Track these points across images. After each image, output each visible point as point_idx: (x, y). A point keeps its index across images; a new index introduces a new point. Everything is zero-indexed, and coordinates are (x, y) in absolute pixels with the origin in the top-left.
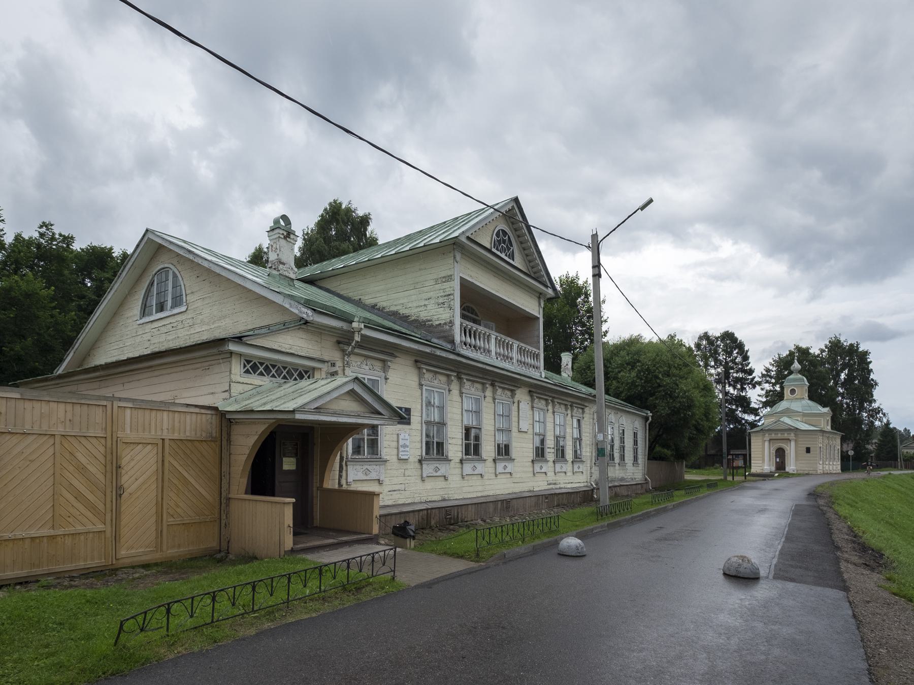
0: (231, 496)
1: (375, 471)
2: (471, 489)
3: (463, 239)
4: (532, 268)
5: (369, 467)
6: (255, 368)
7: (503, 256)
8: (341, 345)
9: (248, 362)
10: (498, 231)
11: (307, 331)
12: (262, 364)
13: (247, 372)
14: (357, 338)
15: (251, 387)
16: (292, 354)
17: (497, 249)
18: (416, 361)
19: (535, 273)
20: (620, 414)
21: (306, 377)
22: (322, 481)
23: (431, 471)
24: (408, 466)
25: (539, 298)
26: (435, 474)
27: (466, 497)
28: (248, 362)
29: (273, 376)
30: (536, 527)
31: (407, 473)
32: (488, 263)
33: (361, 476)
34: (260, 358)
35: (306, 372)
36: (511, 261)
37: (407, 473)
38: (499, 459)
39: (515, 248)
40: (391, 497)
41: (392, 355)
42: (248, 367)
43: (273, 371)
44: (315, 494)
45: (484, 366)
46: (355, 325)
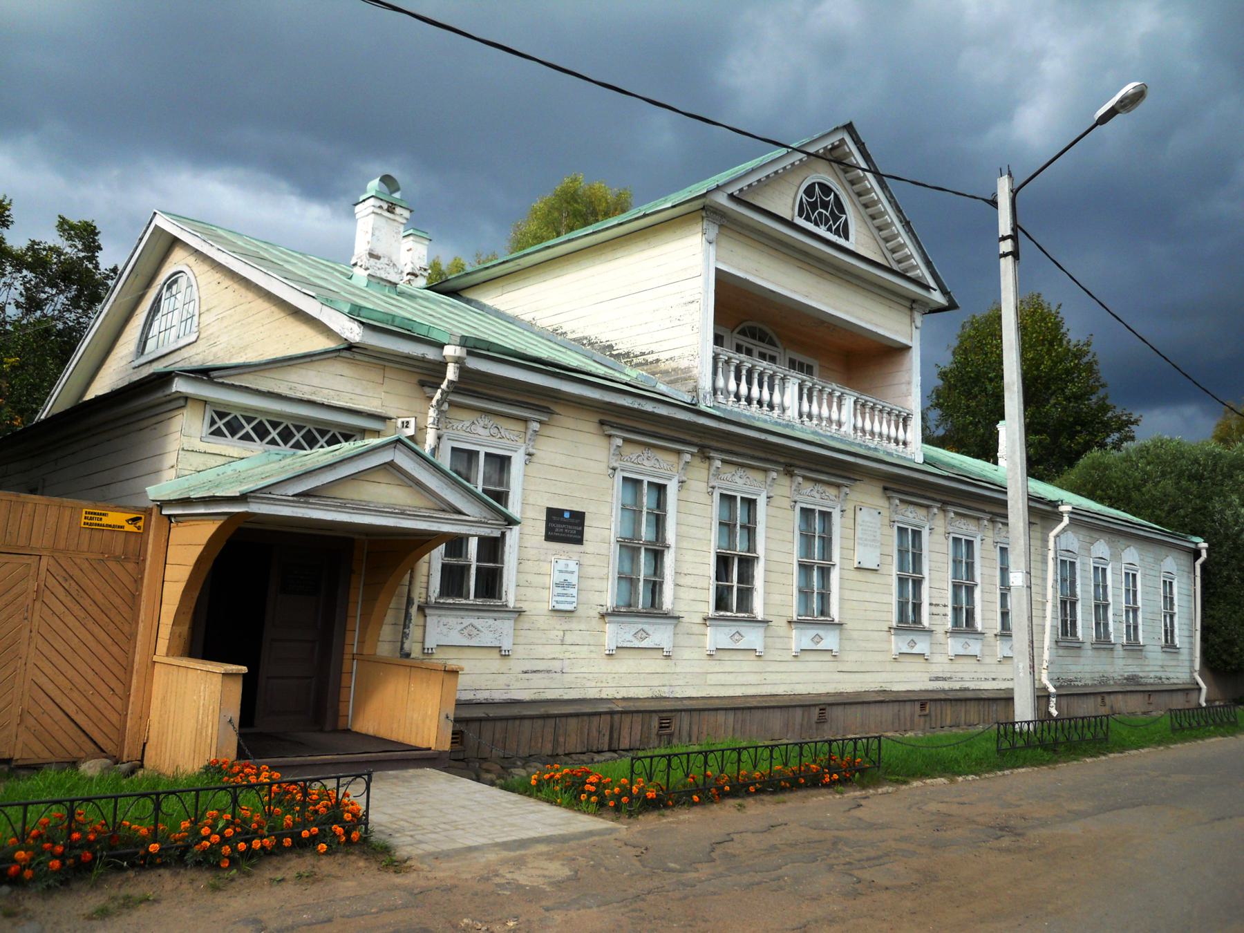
0: (155, 658)
1: (489, 629)
2: (730, 679)
3: (722, 199)
4: (893, 251)
5: (476, 622)
6: (234, 427)
7: (822, 231)
8: (606, 428)
9: (221, 415)
10: (812, 186)
11: (353, 362)
12: (299, 428)
13: (218, 433)
14: (451, 373)
15: (220, 460)
16: (322, 405)
17: (808, 219)
18: (885, 489)
19: (899, 262)
20: (1122, 542)
21: (322, 442)
22: (362, 642)
23: (629, 637)
24: (574, 625)
25: (912, 309)
26: (637, 644)
27: (631, 695)
28: (221, 415)
29: (273, 442)
30: (1099, 728)
31: (569, 638)
32: (858, 277)
33: (456, 638)
34: (246, 409)
35: (323, 433)
36: (841, 241)
37: (569, 638)
38: (438, 606)
39: (852, 215)
40: (526, 684)
41: (549, 412)
42: (220, 424)
43: (274, 434)
44: (345, 668)
45: (763, 436)
46: (449, 351)
